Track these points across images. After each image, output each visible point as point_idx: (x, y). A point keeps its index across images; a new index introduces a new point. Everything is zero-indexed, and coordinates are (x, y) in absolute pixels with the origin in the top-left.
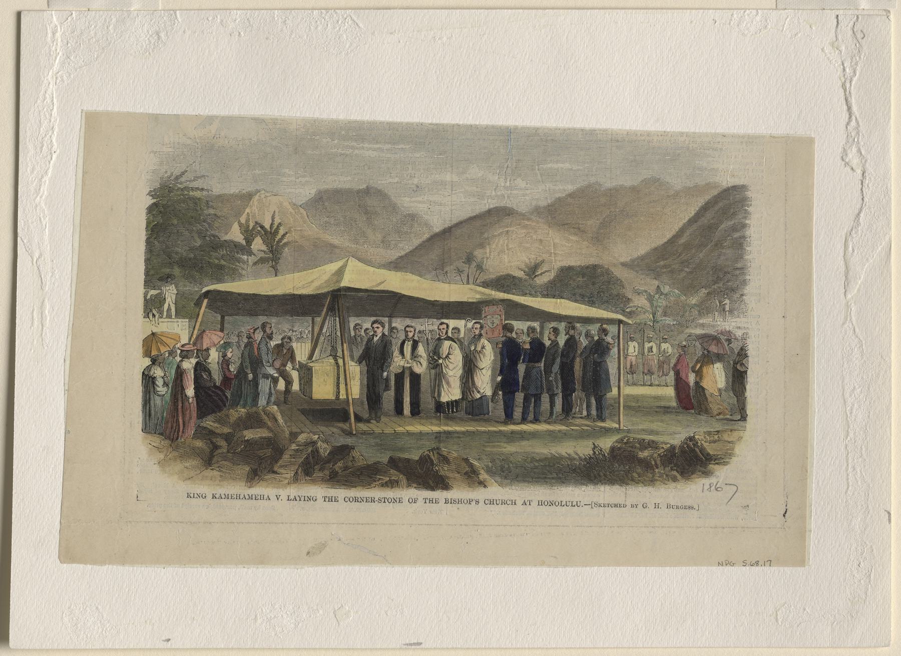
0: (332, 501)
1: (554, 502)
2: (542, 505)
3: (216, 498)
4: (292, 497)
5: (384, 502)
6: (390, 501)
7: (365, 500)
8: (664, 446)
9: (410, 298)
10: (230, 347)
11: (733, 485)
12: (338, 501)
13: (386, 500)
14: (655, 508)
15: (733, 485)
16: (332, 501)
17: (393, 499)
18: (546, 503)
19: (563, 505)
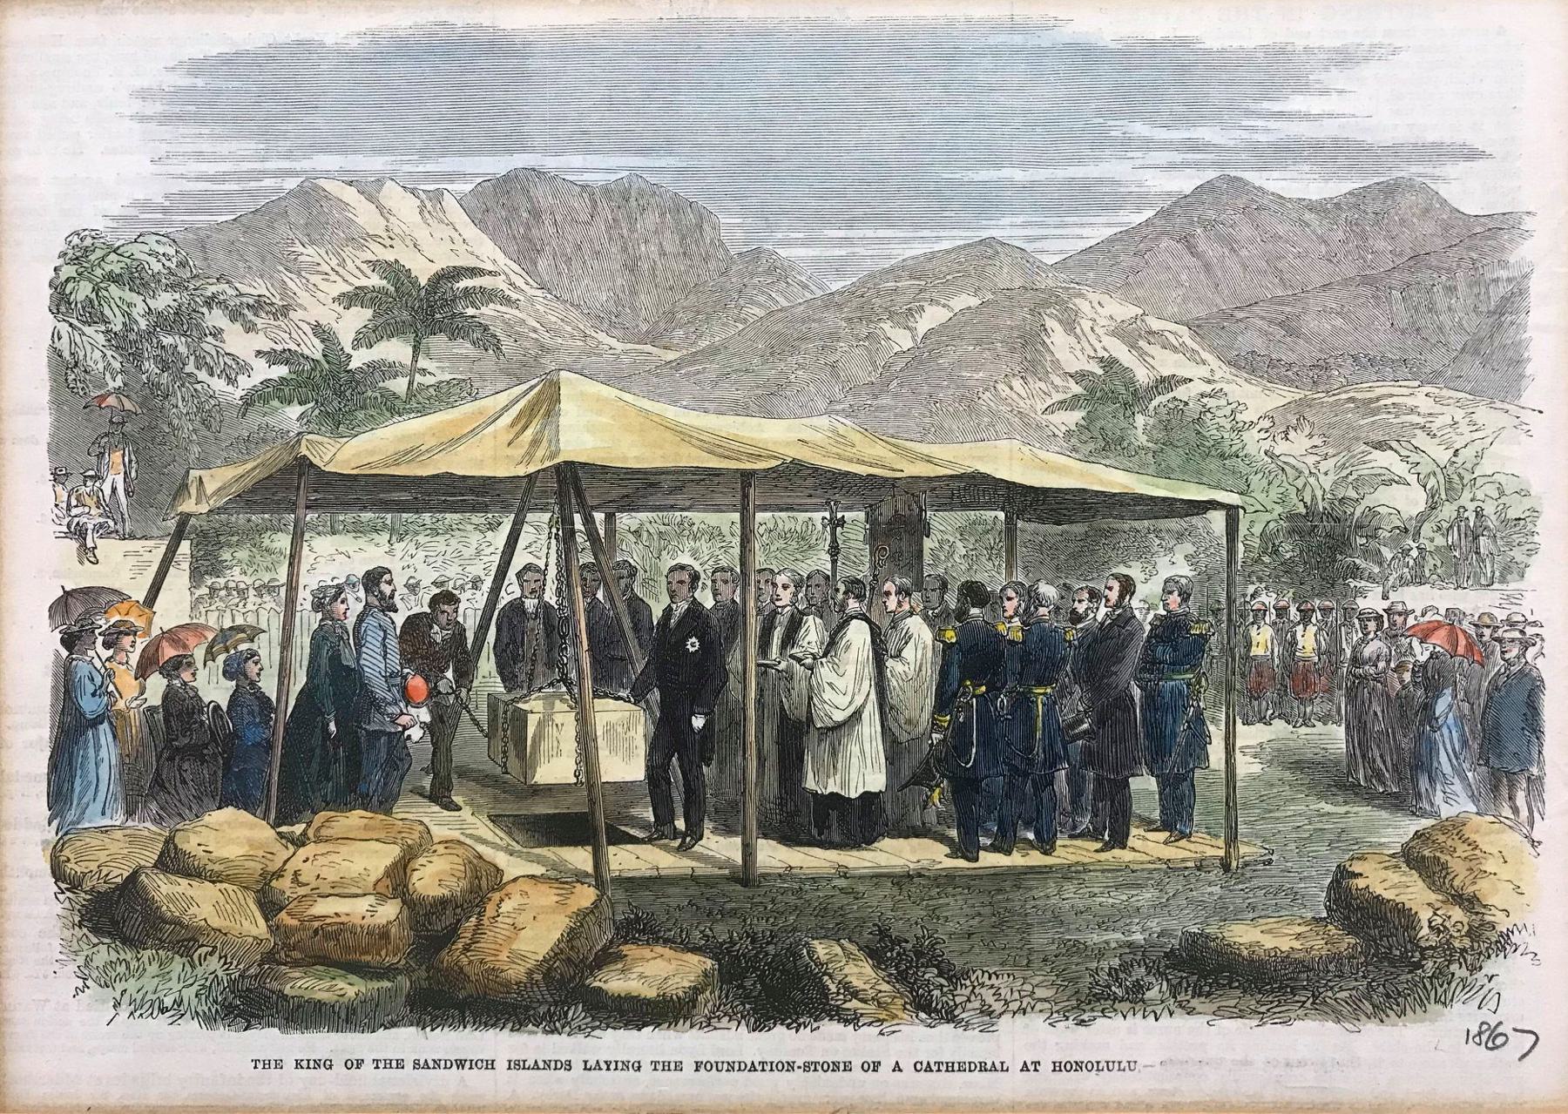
0: (669, 1070)
1: (322, 1062)
2: (1060, 1070)
3: (302, 1068)
4: (592, 1063)
5: (815, 1070)
6: (825, 1067)
7: (842, 1067)
8: (246, 924)
9: (1057, 491)
10: (655, 639)
11: (1530, 1051)
12: (403, 1068)
13: (819, 1068)
14: (509, 1068)
15: (1530, 1051)
16: (669, 1070)
17: (786, 1065)
18: (780, 1067)
19: (1122, 1067)
